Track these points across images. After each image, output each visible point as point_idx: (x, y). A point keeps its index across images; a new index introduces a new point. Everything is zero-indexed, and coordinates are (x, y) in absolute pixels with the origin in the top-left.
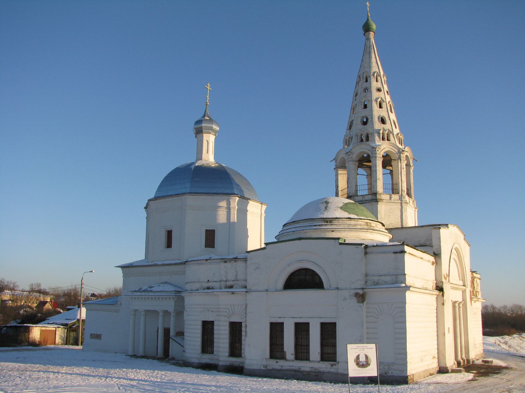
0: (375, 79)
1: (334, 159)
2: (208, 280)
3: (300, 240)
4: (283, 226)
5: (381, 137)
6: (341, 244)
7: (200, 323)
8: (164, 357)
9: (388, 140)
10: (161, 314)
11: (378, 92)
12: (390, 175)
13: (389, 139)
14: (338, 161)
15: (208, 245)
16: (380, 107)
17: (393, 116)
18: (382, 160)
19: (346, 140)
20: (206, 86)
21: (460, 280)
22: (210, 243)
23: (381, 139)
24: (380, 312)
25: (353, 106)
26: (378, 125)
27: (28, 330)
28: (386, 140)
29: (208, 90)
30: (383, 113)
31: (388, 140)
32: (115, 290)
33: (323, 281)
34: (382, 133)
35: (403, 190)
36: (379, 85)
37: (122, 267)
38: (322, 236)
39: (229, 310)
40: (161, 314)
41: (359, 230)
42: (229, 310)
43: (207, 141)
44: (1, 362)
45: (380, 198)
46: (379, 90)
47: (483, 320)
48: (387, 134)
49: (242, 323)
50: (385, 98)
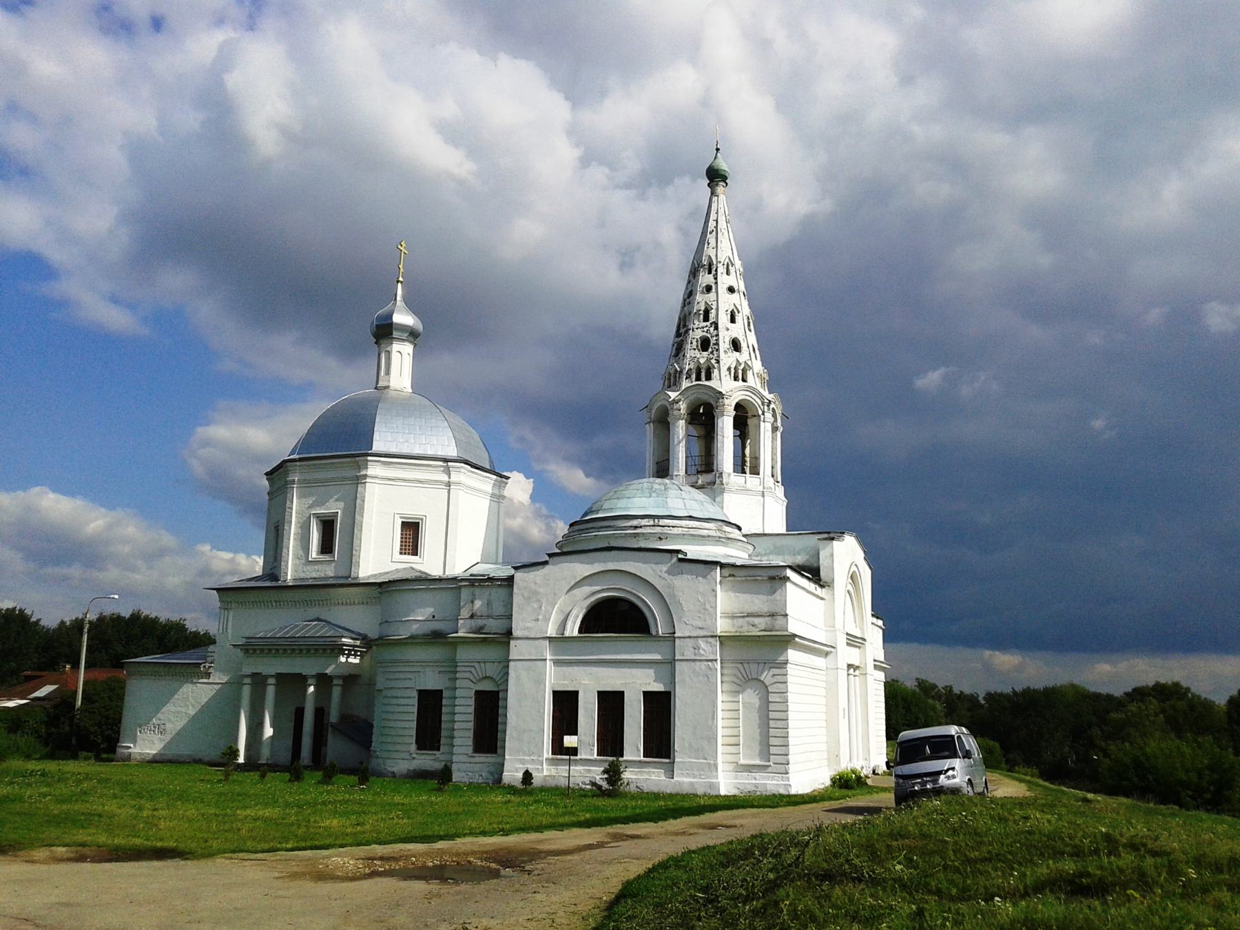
0: (725, 270)
2: (434, 617)
4: (571, 525)
5: (732, 375)
6: (680, 560)
7: (415, 694)
8: (311, 764)
12: (741, 438)
13: (745, 378)
14: (653, 411)
16: (733, 320)
17: (752, 339)
20: (399, 247)
21: (856, 627)
23: (733, 379)
25: (683, 314)
27: (341, 662)
28: (740, 380)
29: (403, 253)
30: (737, 330)
31: (744, 380)
33: (125, 713)
36: (731, 280)
37: (218, 590)
38: (643, 544)
39: (476, 669)
42: (476, 669)
46: (731, 290)
47: (887, 690)
48: (743, 370)
50: (717, 256)
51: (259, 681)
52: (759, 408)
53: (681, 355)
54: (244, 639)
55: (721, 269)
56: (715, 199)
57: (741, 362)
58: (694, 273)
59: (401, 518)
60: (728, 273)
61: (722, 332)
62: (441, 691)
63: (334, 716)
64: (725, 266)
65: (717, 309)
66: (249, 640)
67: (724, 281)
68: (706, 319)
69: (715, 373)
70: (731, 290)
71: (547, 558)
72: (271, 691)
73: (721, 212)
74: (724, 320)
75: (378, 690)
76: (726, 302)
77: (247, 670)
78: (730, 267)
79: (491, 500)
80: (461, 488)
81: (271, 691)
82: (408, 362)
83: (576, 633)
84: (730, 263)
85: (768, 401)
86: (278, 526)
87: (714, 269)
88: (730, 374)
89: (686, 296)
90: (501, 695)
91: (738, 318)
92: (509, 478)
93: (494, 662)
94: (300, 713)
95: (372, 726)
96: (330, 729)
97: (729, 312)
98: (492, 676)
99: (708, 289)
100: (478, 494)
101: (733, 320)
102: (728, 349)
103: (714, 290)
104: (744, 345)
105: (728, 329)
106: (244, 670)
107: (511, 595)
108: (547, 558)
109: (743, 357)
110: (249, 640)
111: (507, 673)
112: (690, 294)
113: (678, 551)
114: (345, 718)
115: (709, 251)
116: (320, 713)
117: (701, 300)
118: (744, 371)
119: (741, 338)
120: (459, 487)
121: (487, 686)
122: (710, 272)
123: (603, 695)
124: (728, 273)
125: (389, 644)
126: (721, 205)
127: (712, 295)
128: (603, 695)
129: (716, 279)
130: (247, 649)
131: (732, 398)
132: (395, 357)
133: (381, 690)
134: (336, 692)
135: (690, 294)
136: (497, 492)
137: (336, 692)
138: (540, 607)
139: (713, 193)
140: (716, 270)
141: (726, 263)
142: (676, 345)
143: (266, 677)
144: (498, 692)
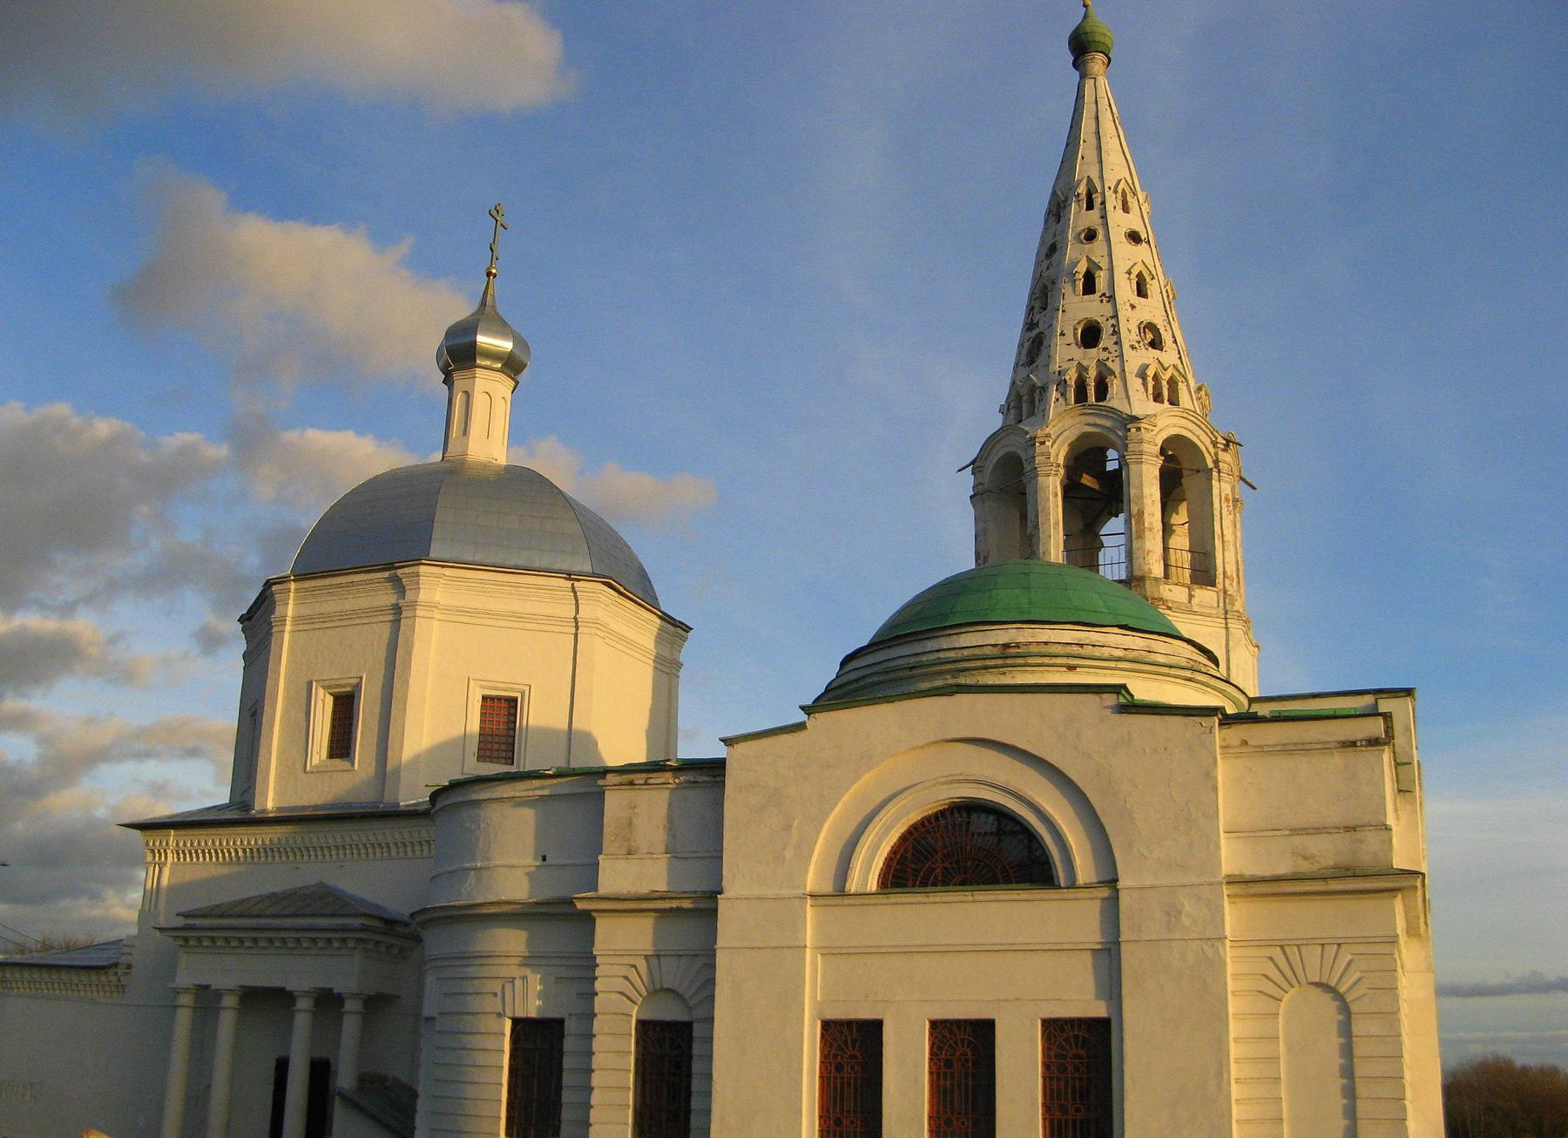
1: (972, 463)
3: (951, 694)
4: (844, 663)
5: (1150, 390)
9: (1174, 401)
10: (304, 1004)
11: (1130, 243)
15: (488, 753)
16: (1141, 291)
18: (1160, 461)
19: (1019, 397)
22: (496, 746)
23: (1151, 397)
24: (1289, 974)
25: (1040, 286)
26: (1138, 358)
30: (1151, 309)
32: (75, 943)
34: (1152, 375)
35: (1229, 574)
36: (1133, 221)
40: (304, 1004)
41: (1166, 670)
43: (466, 392)
44: (687, 1130)
45: (1156, 595)
49: (695, 1026)
51: (207, 999)
52: (1206, 455)
53: (1040, 361)
54: (181, 918)
55: (1112, 201)
56: (1089, 84)
57: (1166, 365)
58: (1057, 211)
59: (482, 687)
60: (1126, 209)
61: (1124, 312)
62: (560, 1022)
63: (345, 1078)
64: (1119, 195)
65: (1111, 269)
66: (191, 921)
67: (1120, 222)
68: (1089, 287)
69: (1115, 386)
70: (1134, 237)
71: (802, 717)
72: (227, 1022)
73: (1103, 103)
74: (1125, 291)
75: (427, 1019)
76: (1127, 257)
77: (185, 979)
78: (1129, 199)
79: (655, 667)
80: (599, 633)
81: (227, 1022)
82: (502, 411)
83: (873, 885)
84: (1127, 191)
85: (1224, 442)
86: (256, 711)
87: (1099, 200)
88: (1146, 391)
89: (1045, 250)
90: (697, 1031)
91: (1153, 288)
92: (692, 629)
93: (680, 956)
94: (282, 1066)
95: (414, 1095)
96: (337, 1098)
97: (1133, 276)
98: (675, 988)
99: (1091, 236)
100: (628, 651)
101: (1141, 291)
102: (1139, 342)
103: (1100, 236)
104: (1166, 337)
105: (1133, 307)
106: (178, 980)
107: (718, 805)
108: (801, 717)
109: (1169, 356)
110: (191, 921)
111: (711, 982)
112: (1052, 249)
113: (1119, 689)
114: (368, 1082)
115: (1084, 169)
116: (320, 1071)
117: (1076, 256)
118: (1172, 383)
119: (1161, 325)
120: (593, 631)
121: (669, 1012)
122: (1090, 206)
123: (942, 1030)
124: (1126, 209)
125: (447, 918)
126: (1101, 93)
127: (1098, 245)
128: (942, 1030)
129: (1104, 217)
130: (186, 939)
131: (1156, 429)
132: (479, 403)
133: (430, 1020)
134: (351, 1026)
135: (1052, 249)
136: (666, 653)
137: (351, 1026)
138: (788, 828)
139: (1083, 76)
140: (1103, 203)
141: (1120, 190)
142: (1027, 345)
143: (218, 994)
144: (688, 1026)
